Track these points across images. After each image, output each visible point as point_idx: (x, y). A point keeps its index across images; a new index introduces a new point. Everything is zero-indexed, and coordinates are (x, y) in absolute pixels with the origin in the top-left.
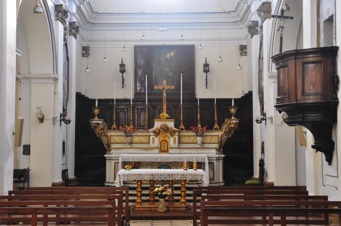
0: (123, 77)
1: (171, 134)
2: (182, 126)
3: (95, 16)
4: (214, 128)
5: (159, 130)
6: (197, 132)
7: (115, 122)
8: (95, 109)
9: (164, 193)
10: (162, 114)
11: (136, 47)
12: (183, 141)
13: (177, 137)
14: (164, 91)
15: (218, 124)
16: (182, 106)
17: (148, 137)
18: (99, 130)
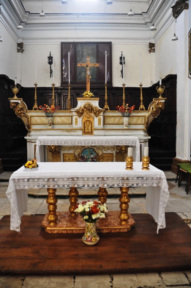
0: (51, 67)
1: (95, 114)
2: (106, 106)
3: (27, 16)
4: (140, 108)
5: (83, 110)
6: (123, 111)
7: (36, 102)
8: (14, 87)
9: (94, 217)
10: (85, 93)
11: (62, 44)
12: (108, 121)
13: (102, 117)
14: (88, 68)
15: (143, 104)
16: (107, 85)
17: (71, 117)
18: (19, 111)
